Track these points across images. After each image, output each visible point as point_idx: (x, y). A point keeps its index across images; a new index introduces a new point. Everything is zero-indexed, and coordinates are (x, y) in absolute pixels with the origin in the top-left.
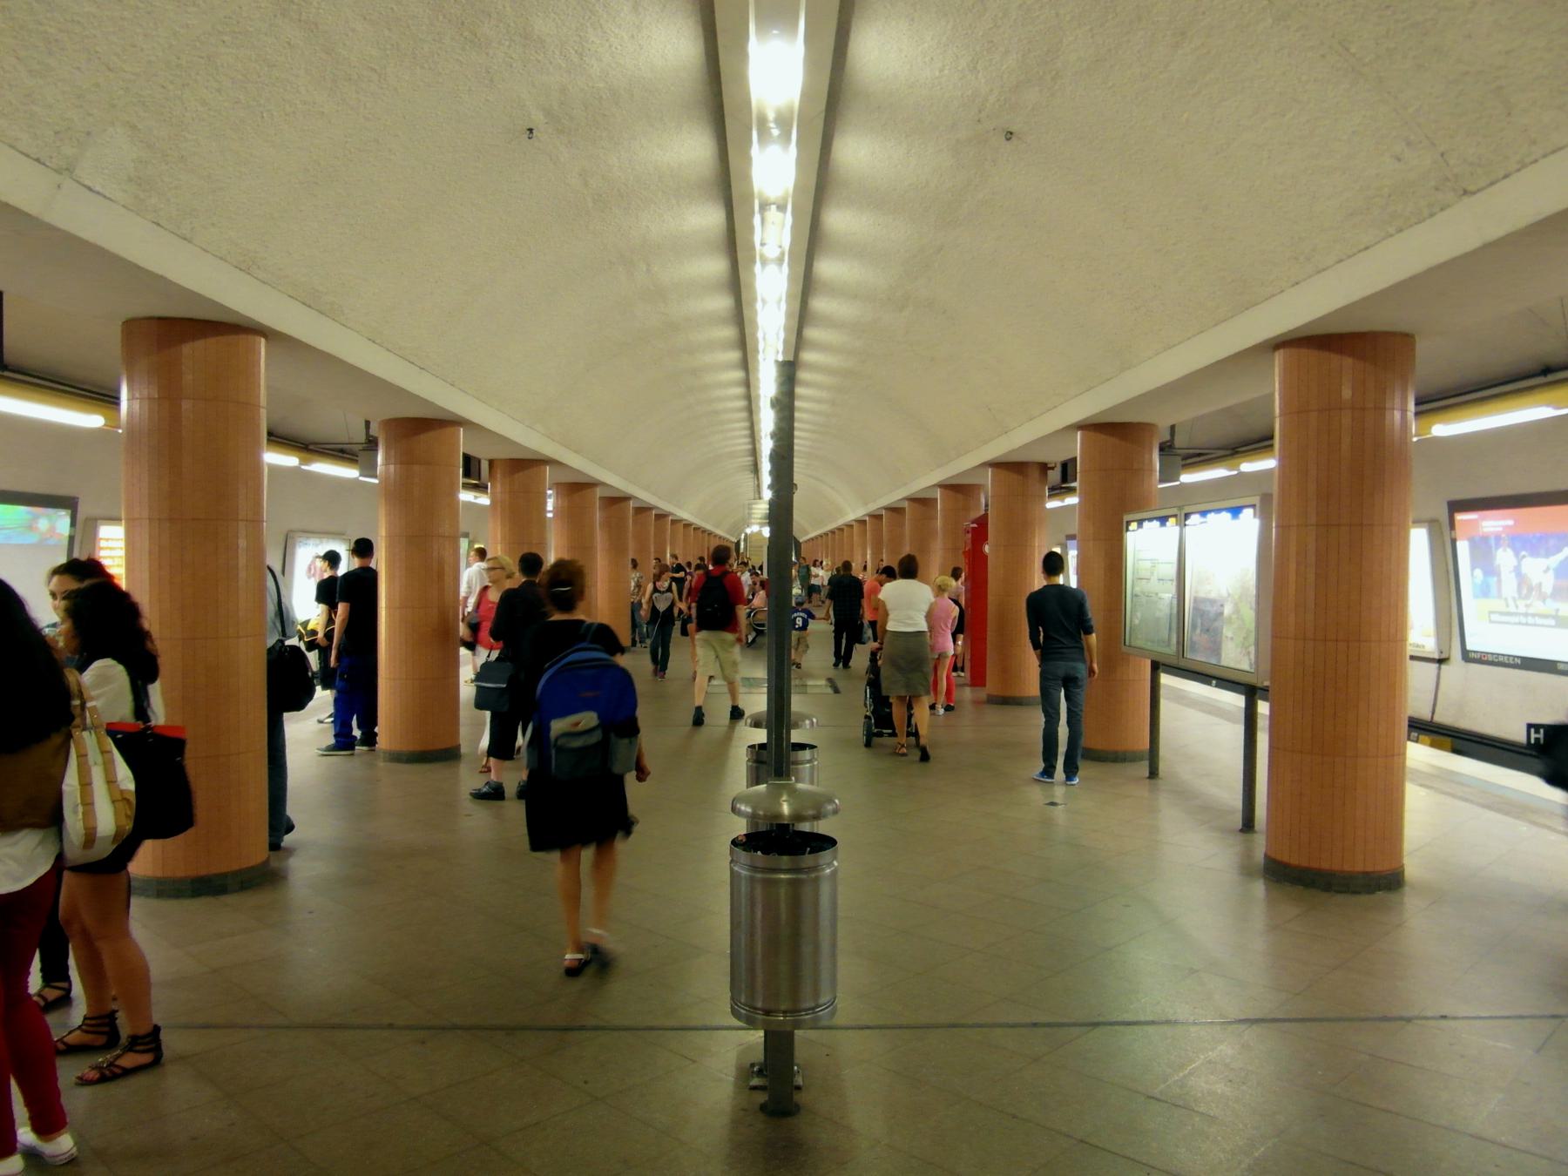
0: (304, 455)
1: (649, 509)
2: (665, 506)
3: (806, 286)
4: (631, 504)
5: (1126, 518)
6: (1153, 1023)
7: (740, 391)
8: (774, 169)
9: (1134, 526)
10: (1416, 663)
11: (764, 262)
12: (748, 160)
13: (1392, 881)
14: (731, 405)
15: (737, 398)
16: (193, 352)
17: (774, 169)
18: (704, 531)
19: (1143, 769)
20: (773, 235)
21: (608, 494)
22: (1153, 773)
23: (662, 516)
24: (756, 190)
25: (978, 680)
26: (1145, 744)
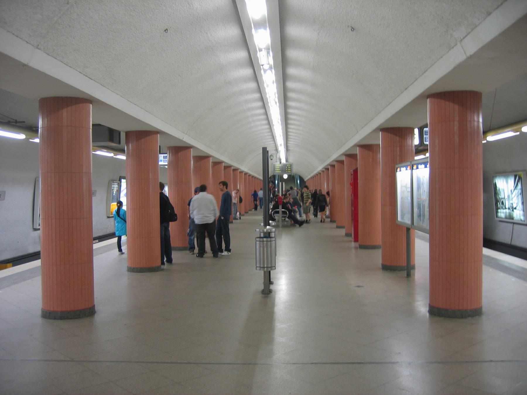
0: (116, 153)
1: (230, 167)
2: (235, 165)
3: (284, 78)
4: (232, 168)
5: (397, 166)
6: (370, 363)
7: (264, 117)
8: (262, 38)
9: (398, 170)
10: (501, 223)
11: (265, 71)
12: (252, 36)
13: (476, 313)
14: (295, 122)
15: (263, 120)
16: (65, 113)
17: (262, 38)
18: (255, 178)
19: (405, 273)
20: (266, 60)
21: (226, 165)
22: (409, 275)
23: (235, 170)
24: (256, 45)
25: (356, 240)
26: (404, 264)
